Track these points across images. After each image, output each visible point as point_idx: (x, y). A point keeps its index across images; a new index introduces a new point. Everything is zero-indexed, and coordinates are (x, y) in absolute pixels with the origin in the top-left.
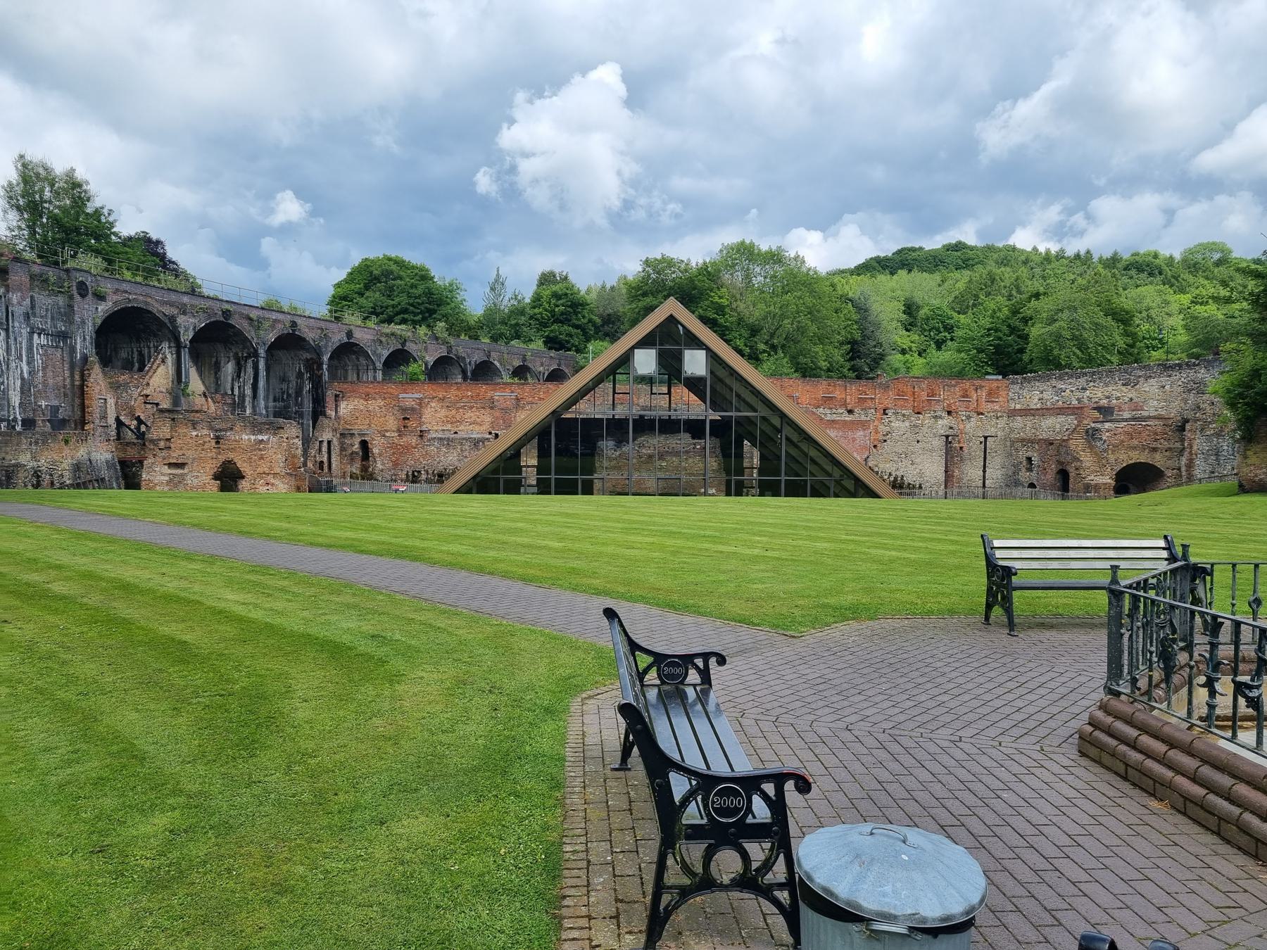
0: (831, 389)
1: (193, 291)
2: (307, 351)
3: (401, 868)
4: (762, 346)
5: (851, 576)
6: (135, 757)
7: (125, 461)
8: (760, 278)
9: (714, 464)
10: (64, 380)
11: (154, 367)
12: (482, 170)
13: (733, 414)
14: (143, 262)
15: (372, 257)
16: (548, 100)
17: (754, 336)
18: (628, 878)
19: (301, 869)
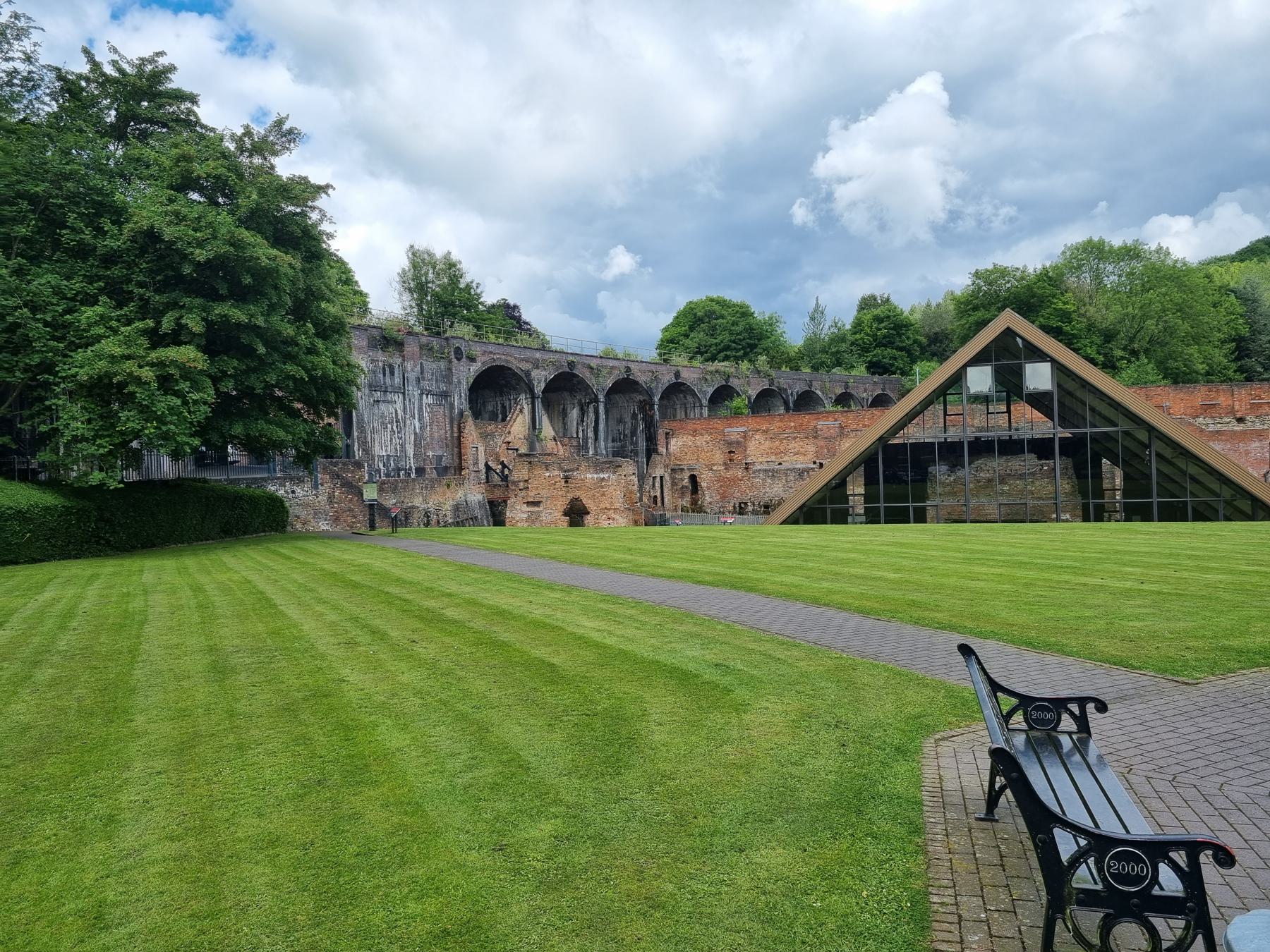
0: (1213, 395)
1: (544, 347)
2: (640, 393)
3: (763, 898)
4: (1119, 353)
5: (1258, 613)
6: (521, 766)
7: (493, 501)
8: (1112, 278)
9: (1066, 486)
10: (446, 432)
11: (514, 417)
12: (799, 201)
13: (1088, 430)
14: (503, 326)
15: (695, 300)
16: (864, 122)
17: (1109, 342)
18: (1007, 940)
19: (670, 887)
